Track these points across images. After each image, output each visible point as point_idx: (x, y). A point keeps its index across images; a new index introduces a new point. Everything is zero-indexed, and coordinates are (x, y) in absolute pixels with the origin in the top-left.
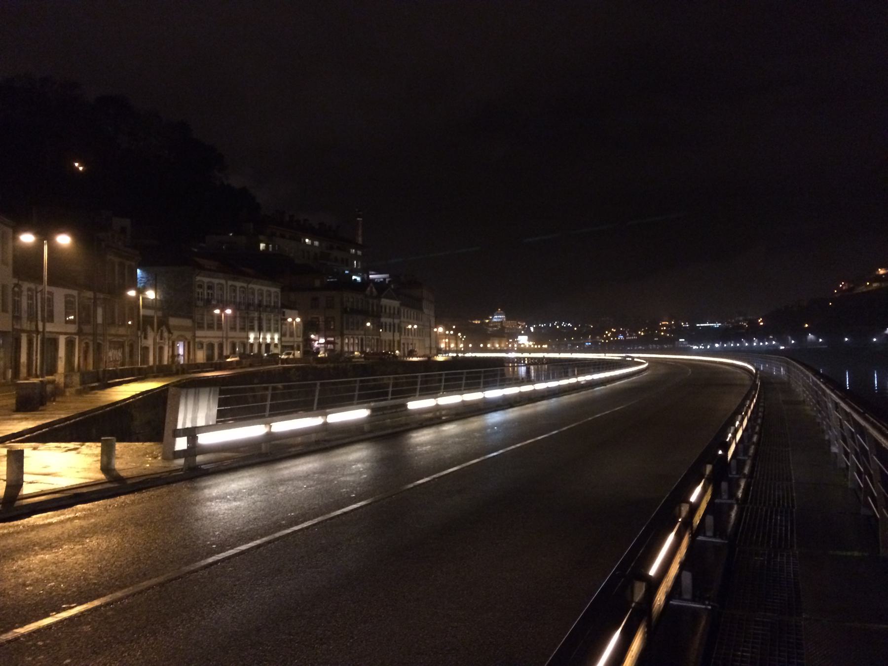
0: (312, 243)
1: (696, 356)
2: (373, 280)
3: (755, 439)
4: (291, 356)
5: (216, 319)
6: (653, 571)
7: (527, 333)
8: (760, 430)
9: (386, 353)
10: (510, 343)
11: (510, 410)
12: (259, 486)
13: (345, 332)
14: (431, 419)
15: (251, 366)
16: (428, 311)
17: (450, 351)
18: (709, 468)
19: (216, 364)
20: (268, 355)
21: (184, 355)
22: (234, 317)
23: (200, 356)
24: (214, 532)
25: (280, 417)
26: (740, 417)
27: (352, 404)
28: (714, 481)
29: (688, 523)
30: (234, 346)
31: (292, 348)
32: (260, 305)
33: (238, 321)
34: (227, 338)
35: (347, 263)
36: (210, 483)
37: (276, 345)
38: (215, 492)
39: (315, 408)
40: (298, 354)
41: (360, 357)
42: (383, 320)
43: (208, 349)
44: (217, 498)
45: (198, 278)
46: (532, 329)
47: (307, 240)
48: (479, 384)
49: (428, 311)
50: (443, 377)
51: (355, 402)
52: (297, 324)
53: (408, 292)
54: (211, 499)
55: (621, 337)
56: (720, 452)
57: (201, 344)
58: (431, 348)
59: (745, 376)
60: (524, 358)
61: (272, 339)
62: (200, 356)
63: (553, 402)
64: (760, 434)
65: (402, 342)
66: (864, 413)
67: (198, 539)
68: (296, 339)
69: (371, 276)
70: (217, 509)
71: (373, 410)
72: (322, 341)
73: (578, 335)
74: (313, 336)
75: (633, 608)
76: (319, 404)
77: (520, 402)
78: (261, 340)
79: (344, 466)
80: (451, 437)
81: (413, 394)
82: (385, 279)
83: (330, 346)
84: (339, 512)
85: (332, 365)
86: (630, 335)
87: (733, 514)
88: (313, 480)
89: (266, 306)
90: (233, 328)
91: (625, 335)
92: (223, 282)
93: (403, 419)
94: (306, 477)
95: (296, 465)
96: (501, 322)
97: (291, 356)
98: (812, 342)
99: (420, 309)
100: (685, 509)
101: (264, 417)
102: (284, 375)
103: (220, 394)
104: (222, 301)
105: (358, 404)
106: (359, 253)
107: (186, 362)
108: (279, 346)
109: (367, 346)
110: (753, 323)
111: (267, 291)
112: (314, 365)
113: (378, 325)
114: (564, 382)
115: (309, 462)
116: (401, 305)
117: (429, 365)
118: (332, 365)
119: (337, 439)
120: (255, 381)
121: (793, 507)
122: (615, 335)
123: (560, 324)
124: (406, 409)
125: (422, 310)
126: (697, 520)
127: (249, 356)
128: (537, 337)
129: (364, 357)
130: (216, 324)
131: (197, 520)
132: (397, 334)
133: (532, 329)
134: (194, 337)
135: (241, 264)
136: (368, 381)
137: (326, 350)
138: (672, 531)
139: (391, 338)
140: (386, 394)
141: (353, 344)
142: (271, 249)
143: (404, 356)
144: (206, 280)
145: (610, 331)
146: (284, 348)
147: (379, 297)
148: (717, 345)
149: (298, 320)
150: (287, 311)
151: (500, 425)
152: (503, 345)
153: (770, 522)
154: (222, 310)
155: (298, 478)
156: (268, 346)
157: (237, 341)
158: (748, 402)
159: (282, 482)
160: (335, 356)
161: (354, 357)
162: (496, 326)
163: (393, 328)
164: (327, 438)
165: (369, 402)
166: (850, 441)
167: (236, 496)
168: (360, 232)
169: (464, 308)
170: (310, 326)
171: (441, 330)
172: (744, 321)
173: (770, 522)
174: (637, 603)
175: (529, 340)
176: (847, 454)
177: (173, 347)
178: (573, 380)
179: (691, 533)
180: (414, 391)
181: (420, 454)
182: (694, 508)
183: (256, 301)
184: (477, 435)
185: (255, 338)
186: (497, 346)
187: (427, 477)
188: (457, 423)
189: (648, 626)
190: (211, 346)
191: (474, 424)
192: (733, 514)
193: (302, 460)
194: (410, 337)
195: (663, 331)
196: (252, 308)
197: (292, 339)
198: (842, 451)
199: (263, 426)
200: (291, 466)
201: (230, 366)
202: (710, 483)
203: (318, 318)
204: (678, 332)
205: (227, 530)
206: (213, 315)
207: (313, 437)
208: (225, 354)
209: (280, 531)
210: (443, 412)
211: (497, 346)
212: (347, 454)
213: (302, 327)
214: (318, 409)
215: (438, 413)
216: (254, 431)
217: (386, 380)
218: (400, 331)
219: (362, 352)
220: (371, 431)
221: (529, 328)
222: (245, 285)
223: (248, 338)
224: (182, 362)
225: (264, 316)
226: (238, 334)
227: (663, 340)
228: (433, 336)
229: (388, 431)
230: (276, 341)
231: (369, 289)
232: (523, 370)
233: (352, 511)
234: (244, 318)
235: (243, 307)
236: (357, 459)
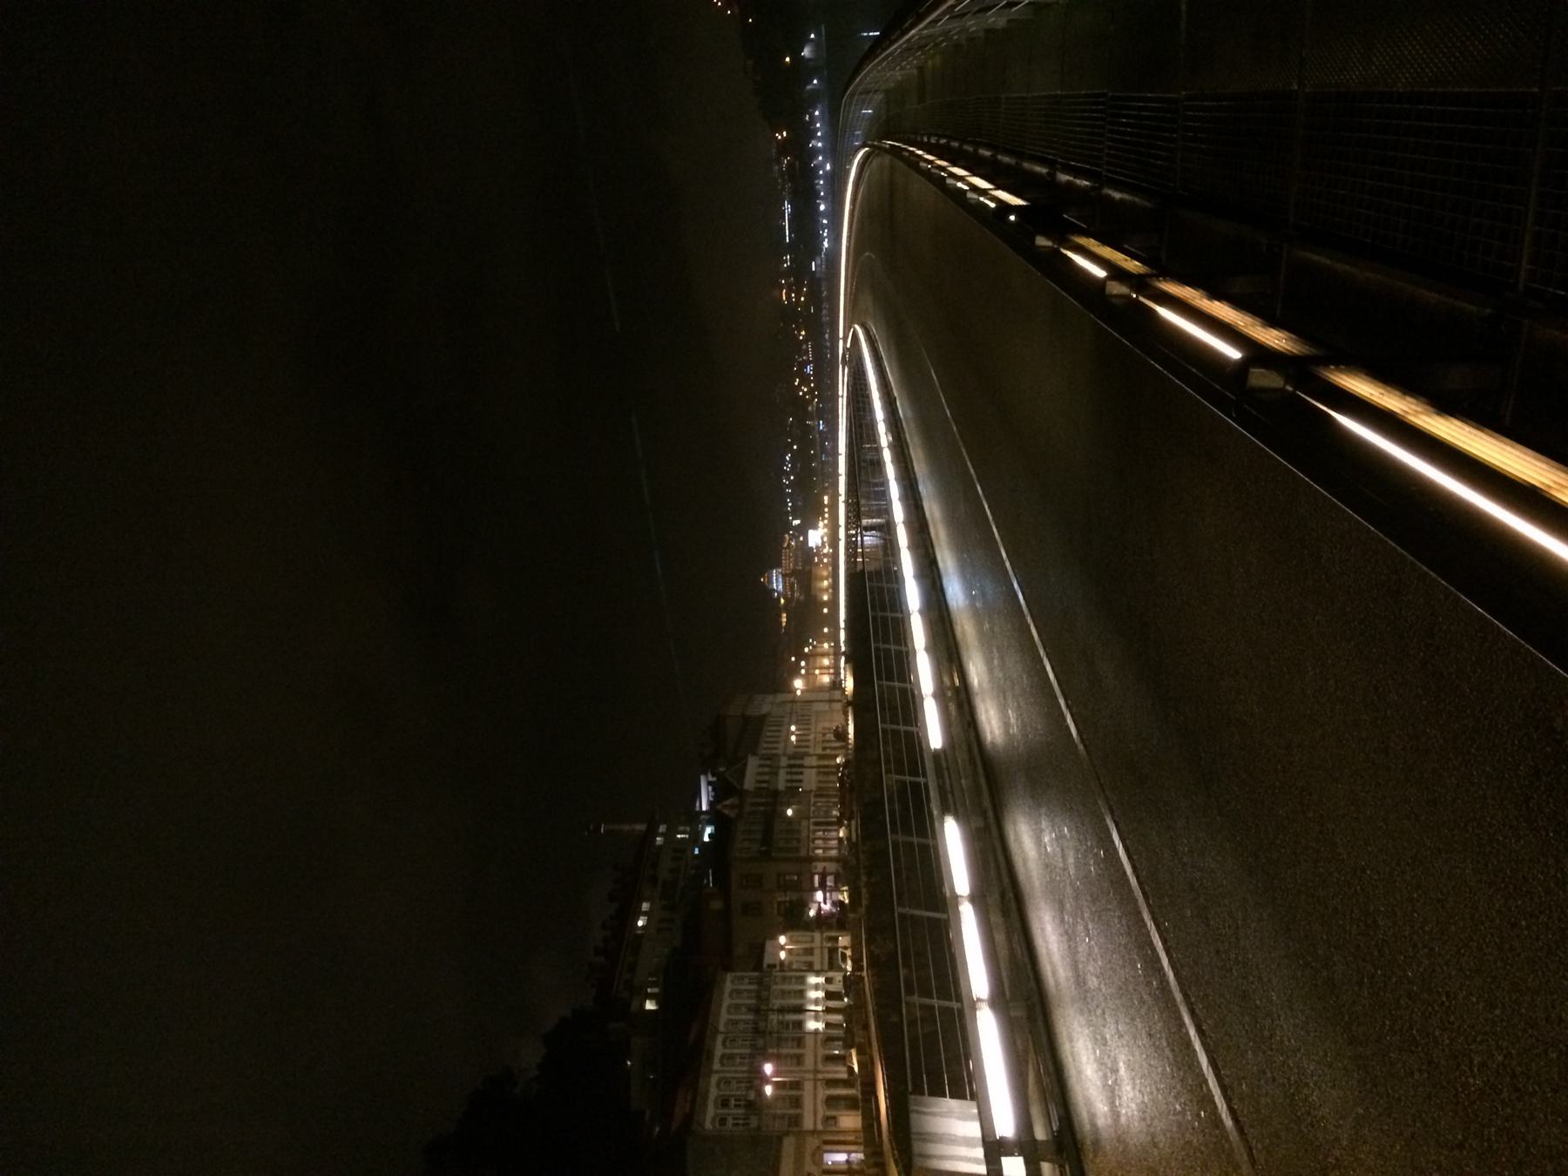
13: (803, 853)
39: (944, 916)
46: (796, 522)
65: (820, 751)
76: (936, 910)
91: (804, 364)
109: (827, 814)
116: (754, 754)
122: (805, 380)
133: (796, 522)
147: (742, 794)
148: (822, 207)
151: (968, 586)
175: (815, 527)
227: (814, 297)
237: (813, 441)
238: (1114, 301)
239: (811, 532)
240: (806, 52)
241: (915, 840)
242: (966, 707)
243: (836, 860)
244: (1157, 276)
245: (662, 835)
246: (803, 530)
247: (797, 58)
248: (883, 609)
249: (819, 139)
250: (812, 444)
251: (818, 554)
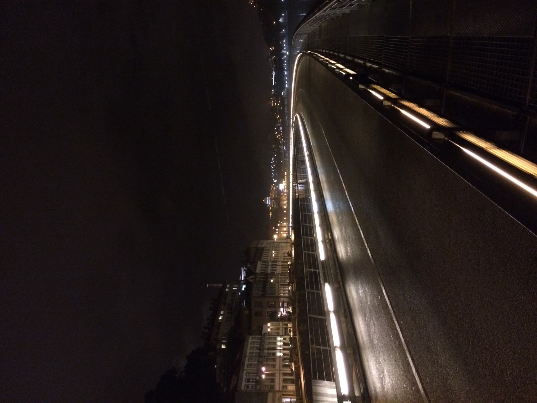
0: (222, 315)
1: (292, 85)
2: (245, 277)
4: (291, 329)
5: (269, 377)
6: (428, 127)
7: (277, 184)
8: (337, 52)
9: (289, 270)
10: (284, 194)
11: (325, 197)
12: (374, 356)
13: (276, 295)
14: (331, 245)
15: (297, 355)
16: (265, 244)
17: (288, 231)
18: (361, 86)
19: (296, 378)
20: (291, 344)
21: (291, 398)
22: (267, 365)
23: (291, 387)
24: (404, 388)
25: (331, 342)
26: (330, 65)
27: (322, 294)
28: (368, 84)
29: (394, 101)
30: (285, 366)
31: (286, 329)
32: (260, 349)
33: (269, 363)
34: (280, 370)
35: (235, 293)
36: (372, 387)
37: (285, 339)
38: (378, 385)
39: (325, 318)
40: (290, 325)
41: (292, 286)
42: (269, 272)
43: (287, 383)
44: (382, 384)
45: (243, 388)
46: (275, 181)
47: (220, 318)
49: (265, 244)
50: (302, 203)
52: (272, 325)
53: (252, 256)
54: (383, 388)
55: (280, 129)
56: (351, 78)
57: (283, 387)
58: (286, 243)
59: (304, 58)
60: (293, 186)
61: (280, 341)
62: (291, 387)
63: (320, 171)
64: (339, 53)
65: (282, 260)
67: (409, 398)
68: (281, 326)
69: (243, 279)
70: (389, 385)
71: (325, 281)
72: (282, 310)
74: (279, 316)
75: (449, 139)
77: (326, 219)
78: (281, 348)
79: (361, 301)
80: (342, 234)
81: (315, 257)
82: (244, 270)
83: (285, 305)
84: (390, 307)
85: (297, 304)
86: (280, 123)
87: (387, 71)
88: (370, 321)
89: (260, 344)
90: (274, 366)
91: (279, 127)
92: (245, 372)
93: (331, 263)
94: (368, 325)
95: (361, 332)
97: (291, 329)
98: (284, 20)
99: (263, 249)
100: (387, 103)
101: (330, 351)
102: (303, 334)
103: (316, 379)
104: (257, 373)
105: (321, 290)
106: (228, 286)
107: (295, 397)
108: (285, 337)
109: (285, 281)
110: (273, 53)
111: (251, 344)
112: (296, 315)
113: (273, 275)
114: (308, 164)
115: (359, 323)
116: (260, 260)
117: (297, 244)
118: (297, 304)
119: (344, 304)
120: (307, 353)
121: (383, 36)
122: (279, 132)
123: (273, 165)
124: (325, 261)
125: (263, 248)
126: (393, 95)
127: (291, 356)
128: (280, 178)
129: (292, 284)
130: (271, 377)
131: (397, 398)
132: (278, 263)
133: (275, 181)
134: (279, 391)
135: (234, 360)
136: (307, 281)
137: (288, 307)
138: (399, 111)
139: (280, 267)
140: (315, 273)
141: (284, 290)
142: (225, 341)
143: (291, 259)
144: (244, 383)
146: (286, 334)
147: (256, 274)
148: (286, 73)
149: (269, 325)
150: (263, 332)
151: (334, 204)
152: (285, 199)
153: (392, 50)
154: (263, 373)
155: (369, 331)
156: (285, 344)
157: (282, 364)
158: (320, 59)
159: (371, 341)
160: (292, 302)
161: (292, 290)
162: (274, 203)
163: (274, 265)
164: (343, 311)
165: (321, 283)
166: (344, 4)
167: (381, 372)
168: (216, 285)
169: (263, 223)
170: (273, 317)
171: (275, 237)
172: (271, 58)
173: (392, 50)
174: (446, 137)
175: (282, 183)
176: (351, 5)
178: (307, 159)
179: (401, 99)
180: (313, 255)
181: (353, 254)
182: (387, 98)
183: (258, 351)
184: (340, 218)
185: (280, 352)
186: (285, 202)
187: (367, 251)
188: (333, 229)
189: (459, 130)
190: (285, 381)
191: (333, 218)
192: (387, 71)
194: (280, 255)
195: (277, 104)
196: (262, 354)
197: (281, 329)
198: (349, 7)
199: (336, 351)
200: (361, 335)
201: (297, 369)
202: (370, 86)
203: (268, 312)
204: (278, 95)
205: (403, 379)
206: (266, 379)
207: (343, 319)
208: (290, 372)
209: (403, 346)
210: (326, 236)
211: (285, 202)
212: (353, 299)
213: (273, 323)
214: (325, 316)
215: (327, 241)
216: (339, 358)
217: (306, 273)
218: (276, 262)
219: (289, 285)
220: (339, 283)
221: (275, 183)
222: (247, 358)
223: (280, 357)
224: (295, 400)
225: (267, 346)
226: (277, 363)
227: (282, 104)
228: (279, 241)
229: (339, 272)
230: (282, 339)
231: (250, 280)
232: (300, 187)
233: (389, 299)
234: (267, 359)
235: (261, 360)
236: (356, 292)
239: (280, 185)
242: (333, 246)
245: (228, 288)
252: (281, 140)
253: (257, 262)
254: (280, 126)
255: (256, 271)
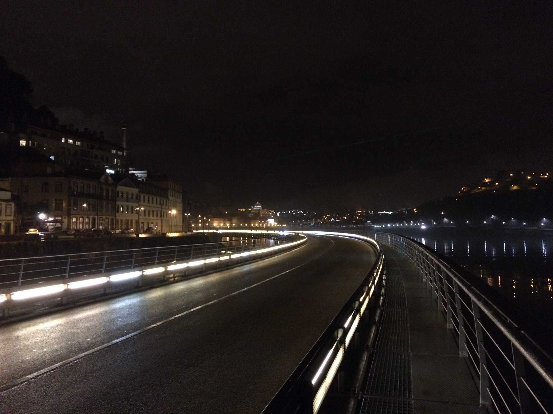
0: (74, 143)
3: (383, 291)
6: (314, 381)
11: (226, 271)
13: (72, 212)
39: (103, 271)
46: (278, 215)
48: (101, 267)
50: (193, 248)
51: (67, 274)
55: (333, 220)
65: (141, 221)
66: (470, 286)
73: (306, 219)
76: (107, 266)
86: (339, 219)
91: (334, 218)
96: (259, 210)
98: (446, 224)
100: (357, 304)
109: (102, 224)
116: (140, 192)
122: (329, 218)
133: (278, 215)
145: (326, 216)
147: (115, 184)
148: (389, 225)
151: (158, 299)
175: (275, 221)
176: (431, 282)
177: (83, 227)
193: (181, 283)
199: (105, 278)
227: (358, 222)
237: (308, 221)
238: (336, 332)
239: (273, 220)
240: (445, 220)
241: (176, 254)
242: (136, 290)
243: (68, 228)
244: (345, 348)
245: (117, 153)
246: (275, 217)
247: (444, 216)
248: (159, 254)
249: (413, 224)
250: (306, 221)
251: (265, 222)
252: (321, 220)
253: (137, 187)
254: (335, 220)
255: (121, 185)
